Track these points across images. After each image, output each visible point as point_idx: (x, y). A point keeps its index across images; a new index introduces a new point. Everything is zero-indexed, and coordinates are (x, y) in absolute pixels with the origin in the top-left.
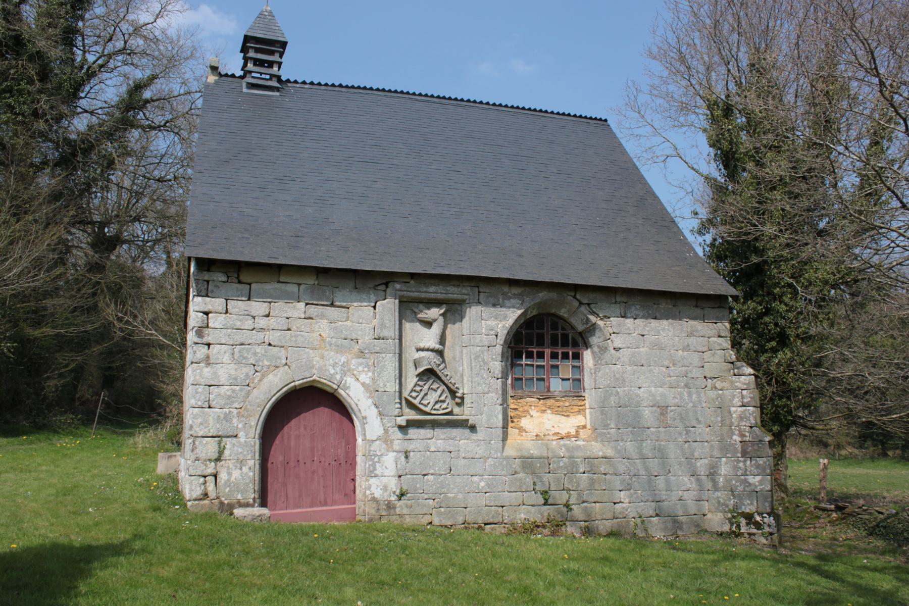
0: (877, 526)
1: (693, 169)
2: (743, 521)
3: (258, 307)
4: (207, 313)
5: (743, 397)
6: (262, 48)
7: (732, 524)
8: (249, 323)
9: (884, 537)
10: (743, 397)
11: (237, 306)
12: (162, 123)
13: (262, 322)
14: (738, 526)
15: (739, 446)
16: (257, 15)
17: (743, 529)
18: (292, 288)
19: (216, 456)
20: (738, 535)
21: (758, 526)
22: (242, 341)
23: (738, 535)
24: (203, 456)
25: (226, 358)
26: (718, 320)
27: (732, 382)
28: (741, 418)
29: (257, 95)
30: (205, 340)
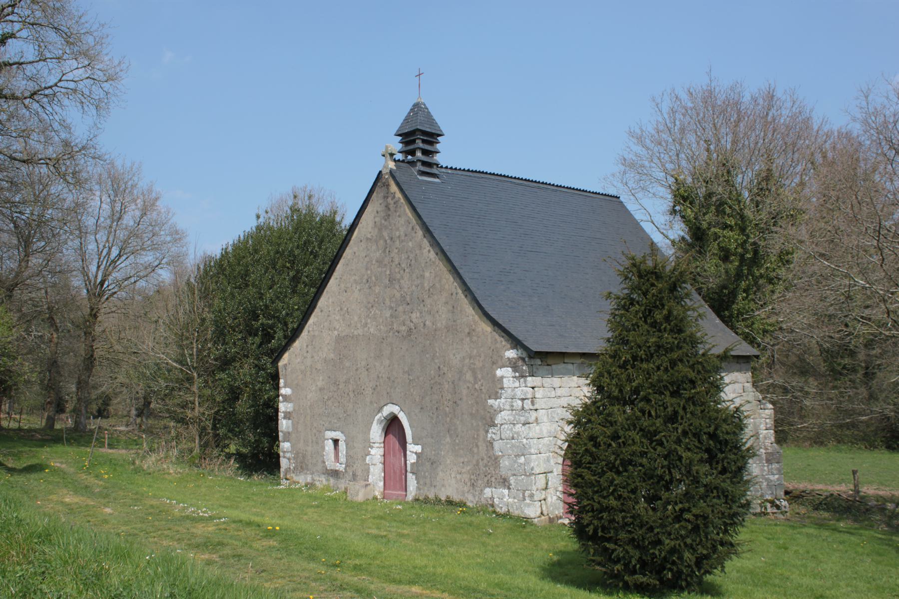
0: (821, 503)
1: (662, 233)
2: (769, 505)
3: (556, 381)
4: (533, 388)
5: (766, 424)
6: (419, 138)
7: (761, 507)
8: (553, 394)
9: (827, 510)
10: (766, 424)
11: (548, 381)
12: (27, 94)
13: (559, 392)
14: (766, 508)
15: (764, 456)
16: (410, 107)
17: (769, 510)
18: (570, 366)
19: (544, 486)
20: (765, 514)
21: (778, 507)
22: (551, 406)
23: (765, 514)
24: (540, 487)
25: (545, 419)
26: (747, 370)
27: (760, 414)
28: (765, 438)
29: (429, 182)
30: (535, 407)
